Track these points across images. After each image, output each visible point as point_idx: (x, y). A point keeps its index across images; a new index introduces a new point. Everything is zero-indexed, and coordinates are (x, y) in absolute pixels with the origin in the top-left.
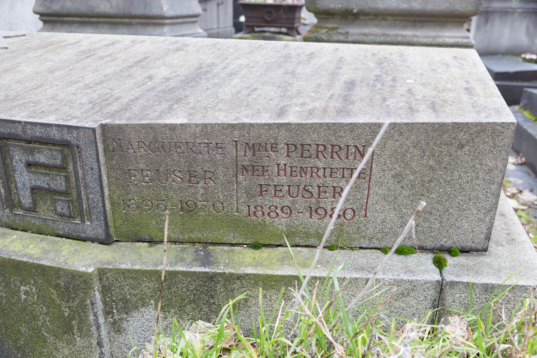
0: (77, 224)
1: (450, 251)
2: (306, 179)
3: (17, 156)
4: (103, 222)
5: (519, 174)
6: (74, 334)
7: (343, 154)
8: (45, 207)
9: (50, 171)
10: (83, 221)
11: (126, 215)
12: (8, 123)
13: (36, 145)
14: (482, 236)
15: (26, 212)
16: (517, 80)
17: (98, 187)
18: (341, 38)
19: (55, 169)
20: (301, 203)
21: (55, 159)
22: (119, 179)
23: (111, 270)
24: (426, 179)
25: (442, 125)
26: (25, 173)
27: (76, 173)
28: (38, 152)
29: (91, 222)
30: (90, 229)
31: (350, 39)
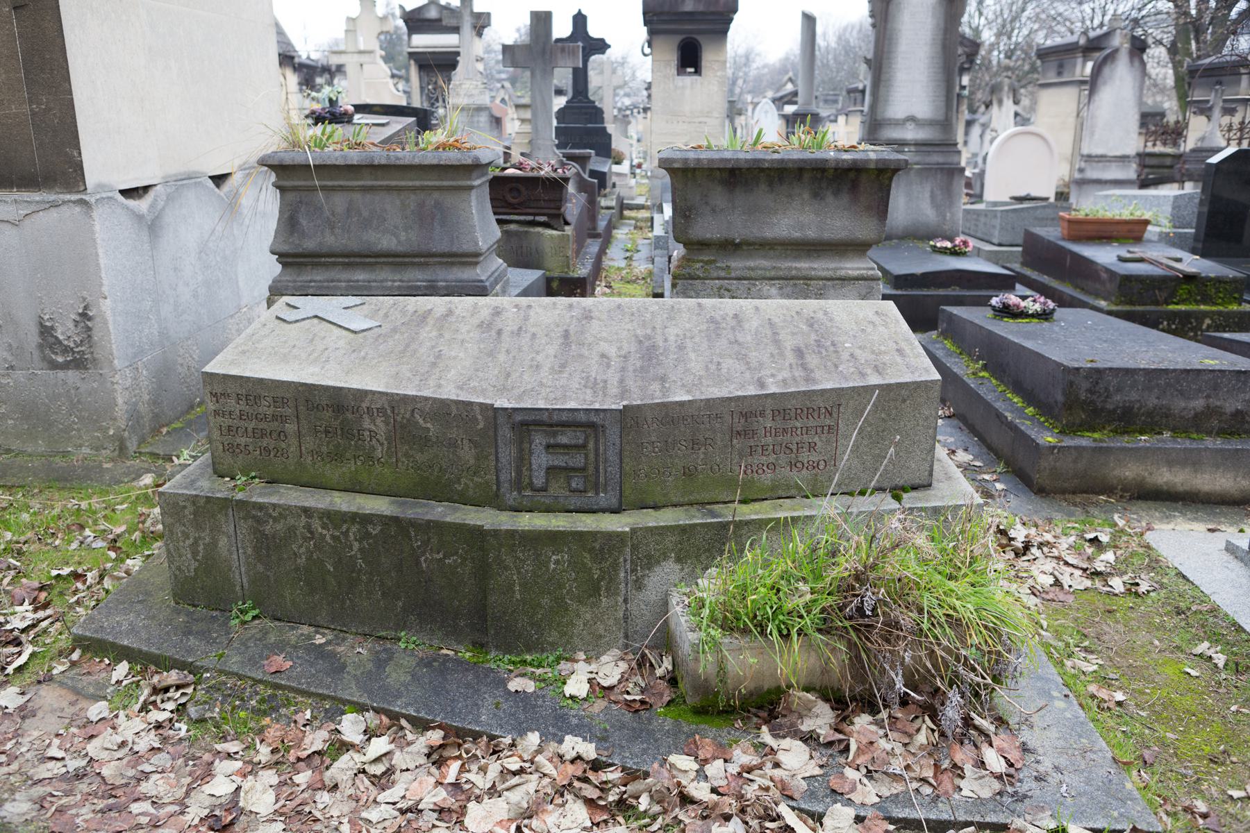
1: (904, 489)
2: (788, 437)
5: (949, 430)
6: (600, 595)
7: (816, 416)
8: (556, 486)
10: (597, 494)
13: (559, 428)
14: (927, 473)
16: (928, 287)
18: (723, 274)
20: (783, 459)
23: (641, 529)
24: (880, 429)
25: (889, 386)
27: (597, 450)
31: (733, 275)
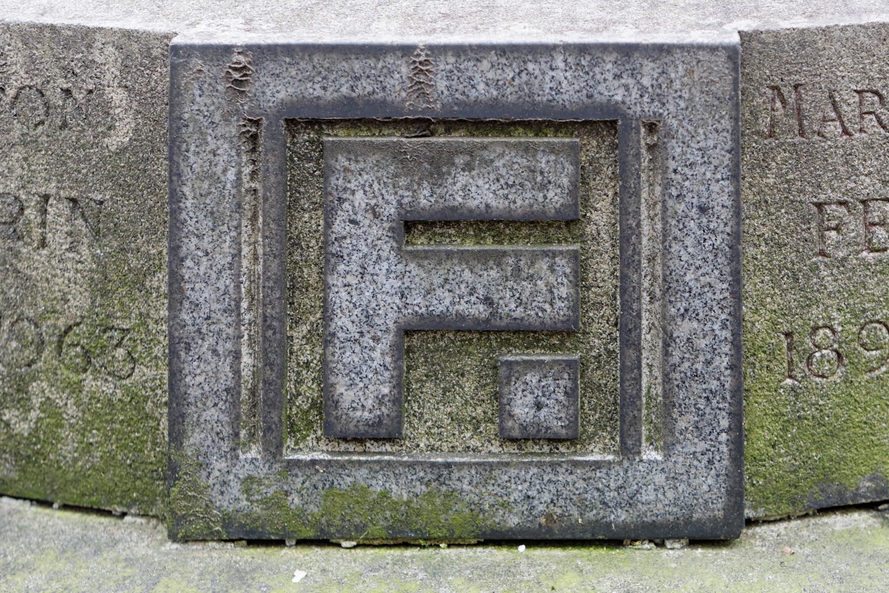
0: (597, 465)
3: (359, 194)
4: (724, 437)
9: (500, 243)
11: (797, 395)
12: (347, 60)
13: (458, 138)
15: (343, 446)
17: (720, 286)
19: (525, 231)
21: (543, 187)
22: (780, 246)
26: (385, 265)
28: (468, 167)
29: (667, 449)
30: (660, 479)
